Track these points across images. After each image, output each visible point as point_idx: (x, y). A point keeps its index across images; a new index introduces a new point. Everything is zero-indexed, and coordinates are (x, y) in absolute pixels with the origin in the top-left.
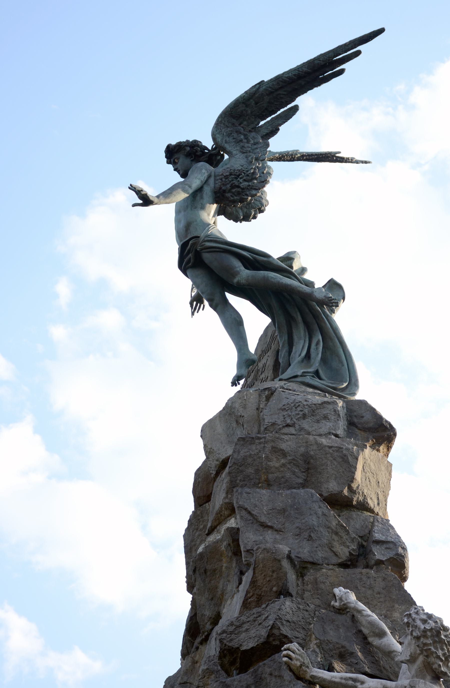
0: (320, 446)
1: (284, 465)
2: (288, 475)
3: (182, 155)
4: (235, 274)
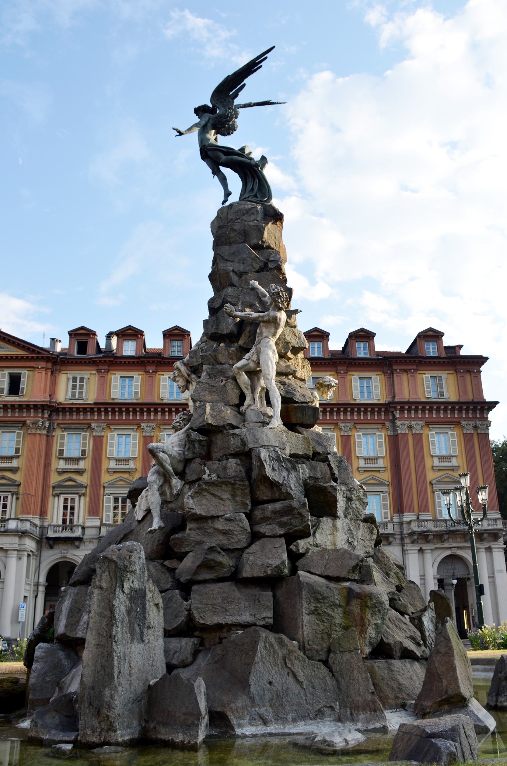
0: (250, 226)
1: (236, 235)
2: (237, 239)
3: (200, 111)
4: (220, 159)
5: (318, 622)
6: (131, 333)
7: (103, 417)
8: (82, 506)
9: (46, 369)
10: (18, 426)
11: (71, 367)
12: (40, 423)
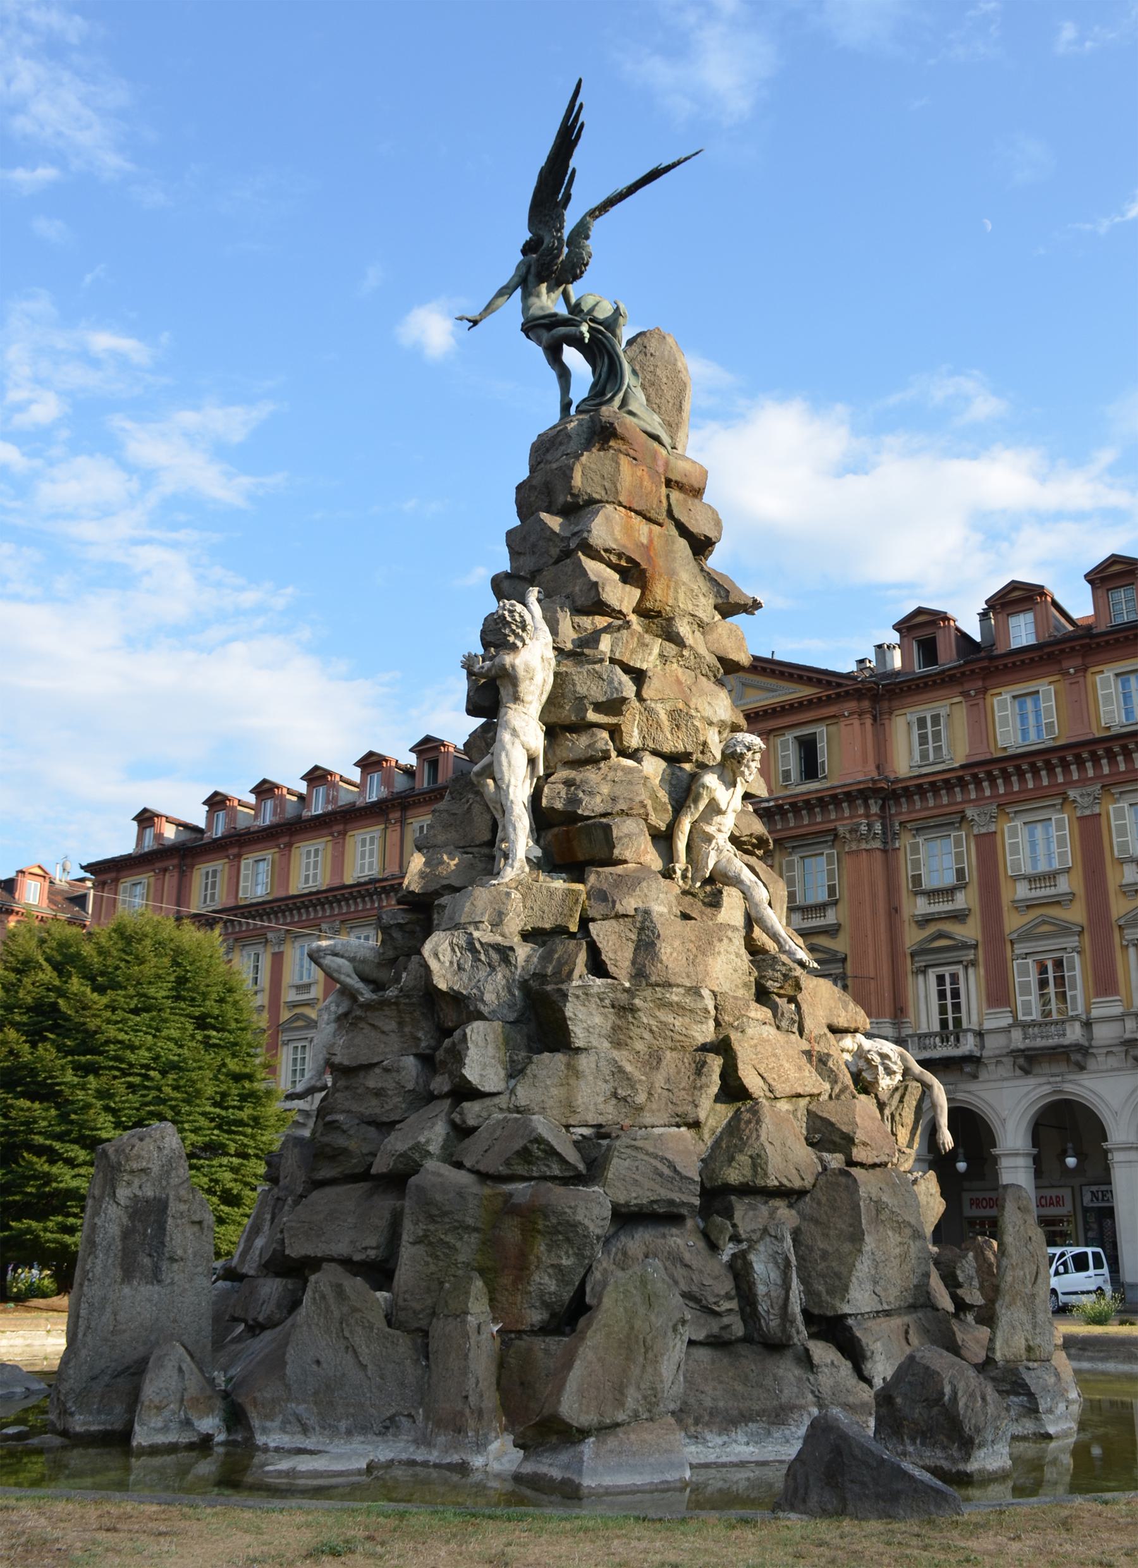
5: (429, 1259)
6: (1016, 598)
7: (988, 793)
8: (973, 986)
9: (861, 714)
10: (826, 842)
11: (910, 700)
12: (864, 829)
